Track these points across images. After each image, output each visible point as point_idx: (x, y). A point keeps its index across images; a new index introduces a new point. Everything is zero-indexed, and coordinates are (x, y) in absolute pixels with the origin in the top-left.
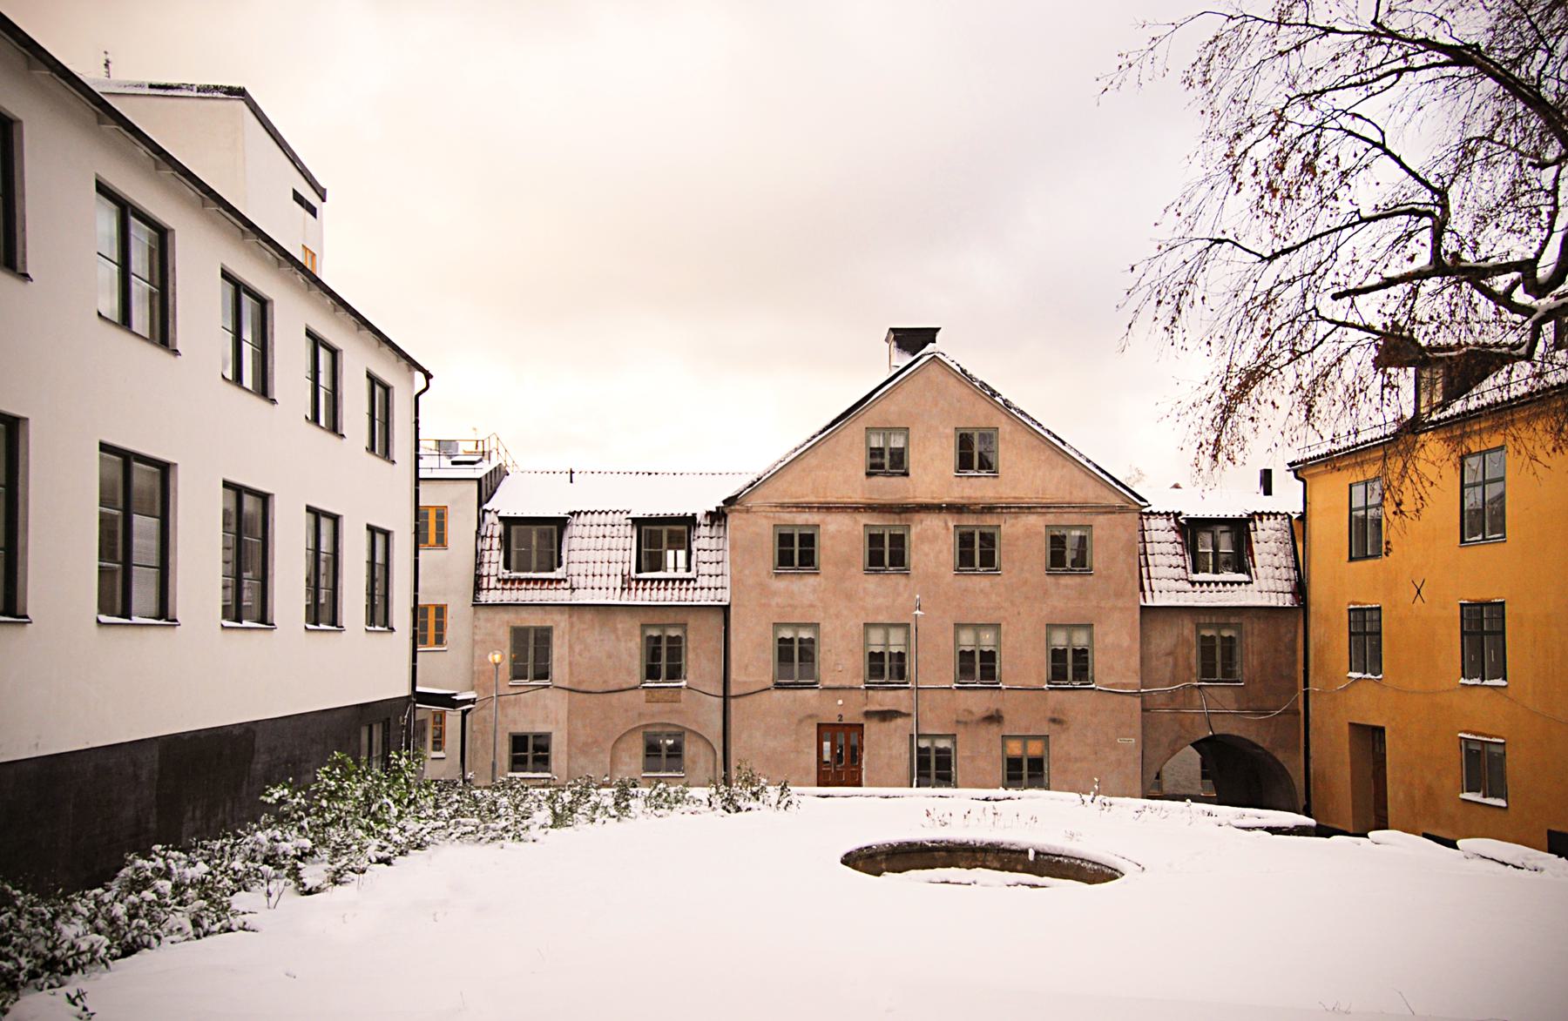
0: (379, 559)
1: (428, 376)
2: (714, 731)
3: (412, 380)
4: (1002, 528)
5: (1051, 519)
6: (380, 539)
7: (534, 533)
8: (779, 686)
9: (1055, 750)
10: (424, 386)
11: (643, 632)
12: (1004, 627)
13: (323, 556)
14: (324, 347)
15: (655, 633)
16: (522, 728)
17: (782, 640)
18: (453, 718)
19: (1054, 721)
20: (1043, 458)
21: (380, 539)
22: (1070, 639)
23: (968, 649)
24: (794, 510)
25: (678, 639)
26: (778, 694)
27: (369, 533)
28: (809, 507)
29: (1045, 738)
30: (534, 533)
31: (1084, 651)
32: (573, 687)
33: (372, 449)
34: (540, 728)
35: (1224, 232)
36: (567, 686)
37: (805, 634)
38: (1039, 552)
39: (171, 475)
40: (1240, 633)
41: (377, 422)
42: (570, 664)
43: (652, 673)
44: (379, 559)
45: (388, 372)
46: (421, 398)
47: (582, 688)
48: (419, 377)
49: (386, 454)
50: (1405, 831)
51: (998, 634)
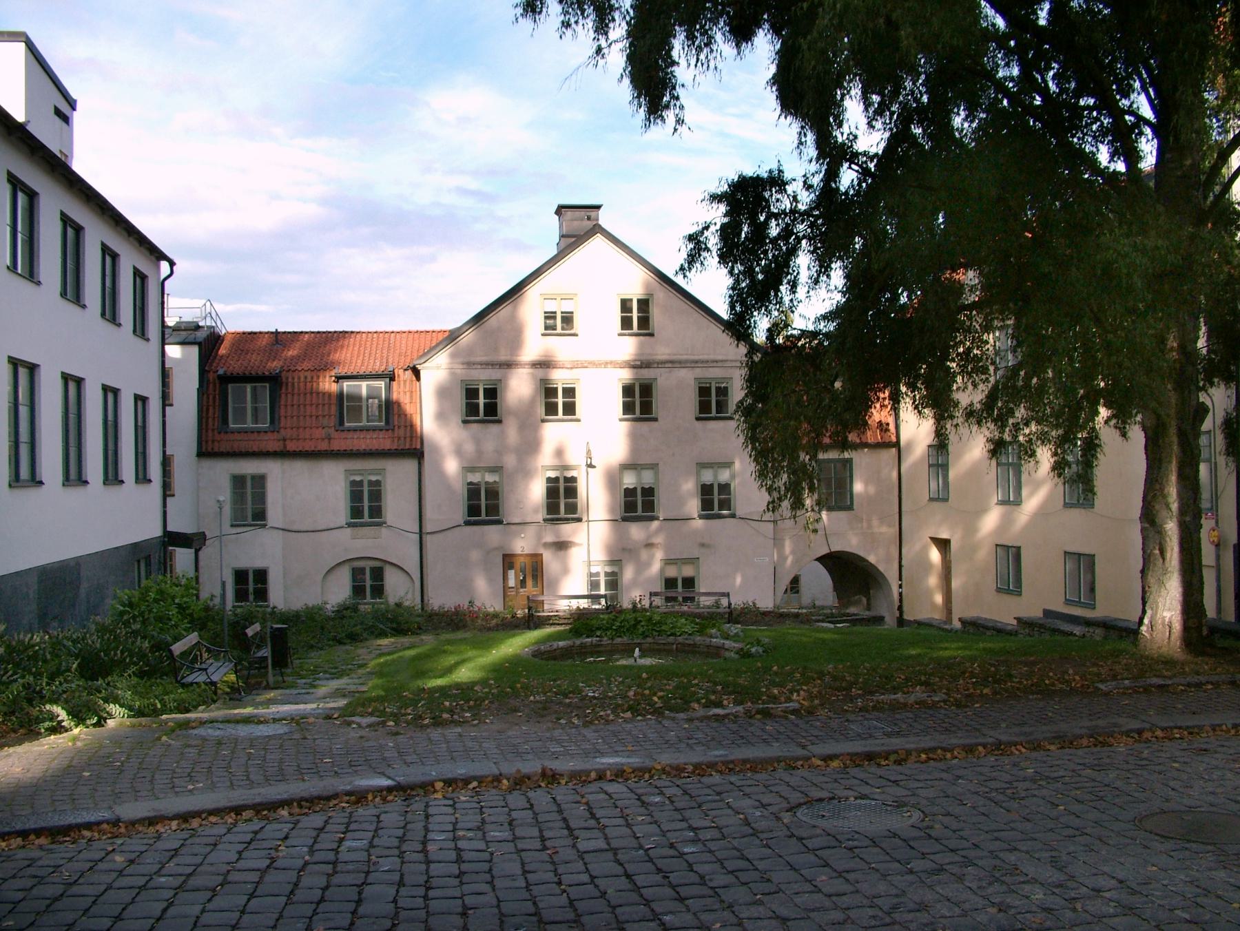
0: (110, 417)
1: (172, 264)
2: (413, 566)
3: (158, 268)
5: (699, 373)
6: (23, 373)
7: (249, 390)
8: (467, 523)
10: (169, 272)
11: (346, 478)
12: (661, 467)
13: (110, 423)
14: (71, 227)
15: (358, 478)
16: (243, 563)
19: (703, 545)
21: (23, 373)
22: (716, 476)
23: (631, 487)
25: (378, 483)
26: (469, 529)
27: (11, 366)
28: (492, 365)
29: (693, 561)
30: (249, 390)
32: (286, 527)
33: (13, 268)
34: (259, 564)
37: (490, 478)
38: (691, 401)
39: (36, 373)
40: (501, 476)
41: (19, 235)
43: (356, 512)
44: (110, 417)
45: (145, 267)
46: (166, 283)
48: (165, 266)
49: (31, 275)
51: (656, 474)
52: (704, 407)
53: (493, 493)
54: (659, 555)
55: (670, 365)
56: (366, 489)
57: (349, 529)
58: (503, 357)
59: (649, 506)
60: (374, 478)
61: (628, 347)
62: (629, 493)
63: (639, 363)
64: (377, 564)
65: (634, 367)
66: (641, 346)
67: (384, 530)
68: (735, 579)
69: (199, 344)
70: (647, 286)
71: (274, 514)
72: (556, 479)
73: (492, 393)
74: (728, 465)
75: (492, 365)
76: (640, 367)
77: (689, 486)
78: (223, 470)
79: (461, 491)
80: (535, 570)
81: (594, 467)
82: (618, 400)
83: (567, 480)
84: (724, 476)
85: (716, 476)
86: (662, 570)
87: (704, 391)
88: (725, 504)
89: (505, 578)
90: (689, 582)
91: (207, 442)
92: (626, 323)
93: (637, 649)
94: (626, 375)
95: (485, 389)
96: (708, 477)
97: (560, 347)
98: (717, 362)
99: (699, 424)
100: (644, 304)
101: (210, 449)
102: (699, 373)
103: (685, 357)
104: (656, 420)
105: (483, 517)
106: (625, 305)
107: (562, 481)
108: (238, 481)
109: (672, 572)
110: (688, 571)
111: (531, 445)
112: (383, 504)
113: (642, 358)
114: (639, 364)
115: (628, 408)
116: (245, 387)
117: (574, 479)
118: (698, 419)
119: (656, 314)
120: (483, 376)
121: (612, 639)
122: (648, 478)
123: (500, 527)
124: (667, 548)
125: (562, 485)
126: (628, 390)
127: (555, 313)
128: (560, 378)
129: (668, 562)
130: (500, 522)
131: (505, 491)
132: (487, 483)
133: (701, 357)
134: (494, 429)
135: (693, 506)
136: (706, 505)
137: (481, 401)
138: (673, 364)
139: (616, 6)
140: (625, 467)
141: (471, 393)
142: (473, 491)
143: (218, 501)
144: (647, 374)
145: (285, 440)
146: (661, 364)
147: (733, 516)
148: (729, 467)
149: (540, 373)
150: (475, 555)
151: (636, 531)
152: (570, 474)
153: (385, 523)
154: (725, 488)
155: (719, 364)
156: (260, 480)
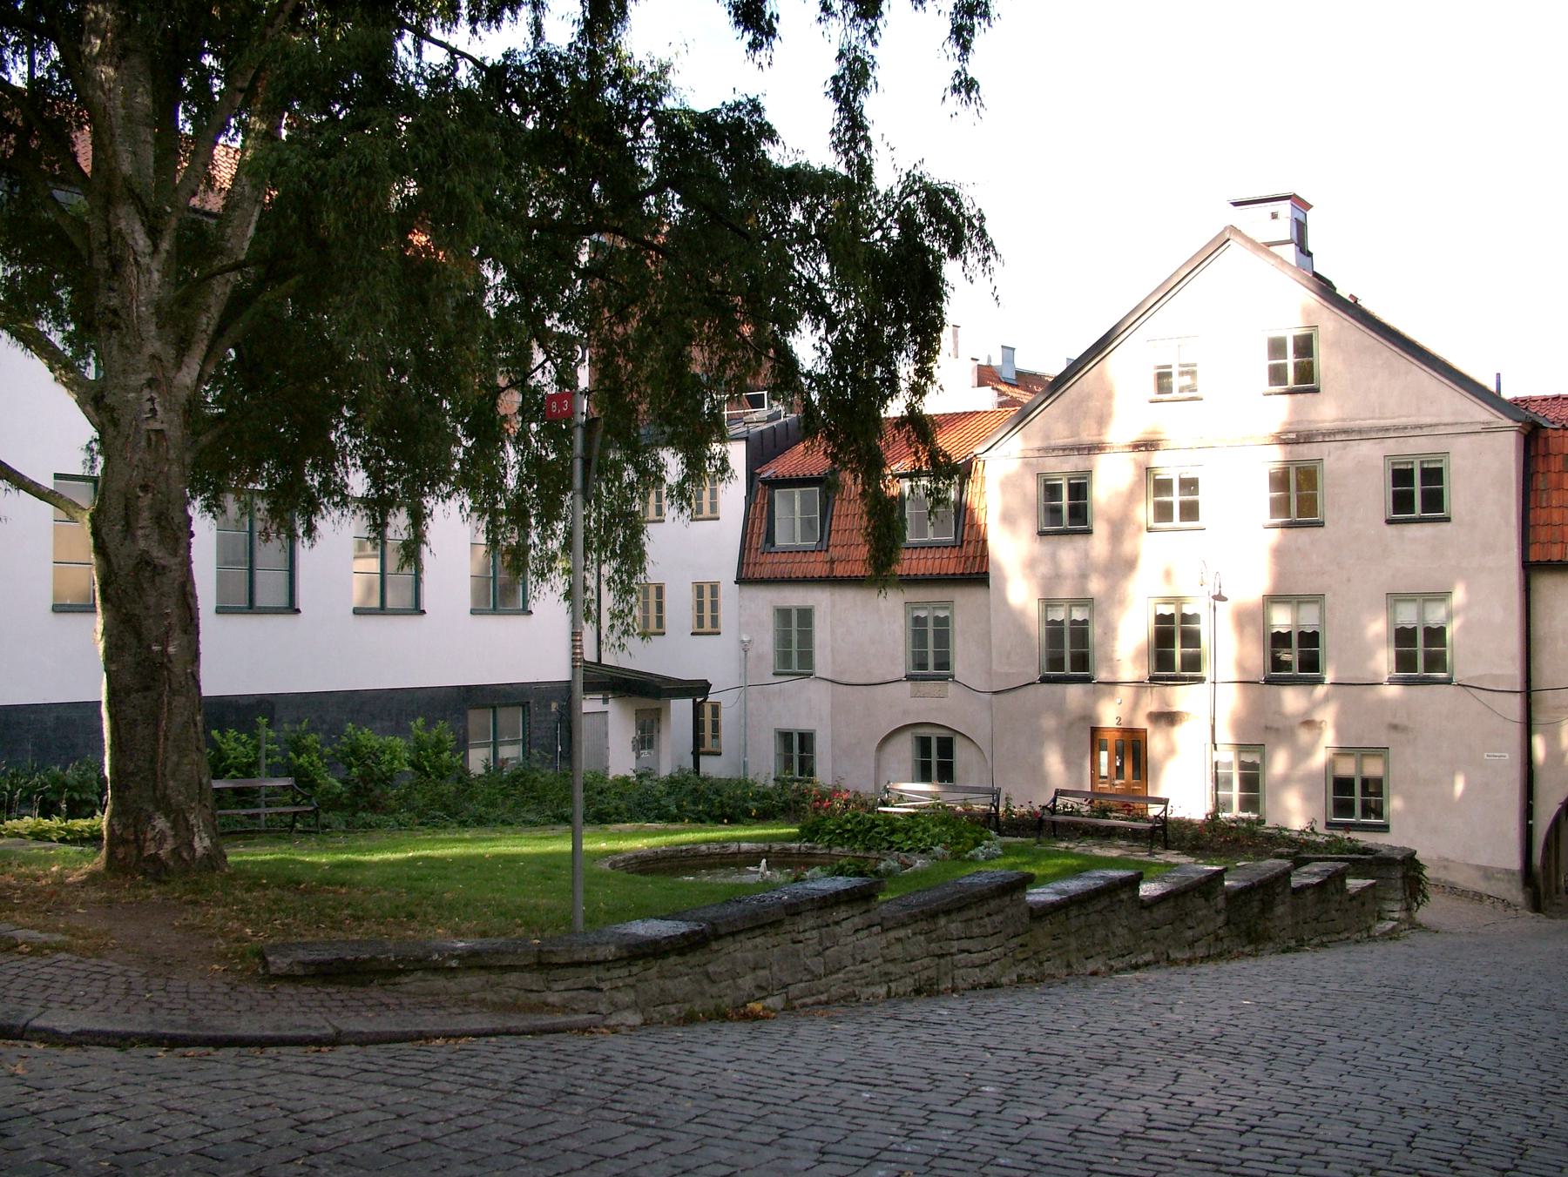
4: (1325, 462)
9: (1396, 771)
11: (906, 613)
15: (923, 614)
17: (1053, 622)
18: (681, 709)
20: (1379, 362)
22: (1421, 613)
23: (1284, 631)
24: (1061, 453)
26: (1046, 687)
28: (1079, 449)
29: (1380, 752)
31: (1315, 635)
34: (804, 726)
35: (1274, 216)
36: (829, 677)
37: (1078, 615)
38: (1379, 492)
42: (832, 651)
47: (845, 680)
50: (198, 634)
52: (1402, 502)
53: (1081, 632)
54: (1328, 738)
55: (1343, 437)
56: (930, 628)
57: (908, 685)
58: (1087, 437)
59: (1311, 663)
60: (942, 614)
61: (1280, 411)
62: (1280, 640)
63: (1293, 436)
64: (944, 733)
65: (1286, 443)
66: (1295, 410)
67: (951, 687)
68: (1452, 783)
69: (747, 439)
70: (1307, 313)
71: (823, 661)
72: (1169, 619)
73: (1080, 490)
74: (1443, 596)
75: (1079, 449)
76: (1296, 442)
77: (1378, 628)
78: (767, 600)
79: (1037, 630)
80: (1133, 747)
81: (1225, 599)
82: (1263, 495)
83: (1185, 618)
84: (1435, 616)
85: (1421, 613)
86: (1330, 765)
87: (1401, 477)
88: (1436, 661)
89: (1095, 763)
90: (1374, 787)
91: (748, 565)
92: (1277, 375)
93: (764, 861)
94: (1276, 456)
95: (1070, 486)
96: (1407, 616)
97: (1166, 420)
98: (1420, 427)
99: (1392, 529)
100: (1305, 346)
101: (750, 575)
102: (1392, 447)
103: (1369, 423)
104: (1321, 524)
105: (1068, 671)
106: (1277, 347)
107: (1177, 619)
108: (783, 614)
109: (1347, 768)
110: (1373, 768)
111: (1121, 566)
112: (951, 650)
113: (1300, 428)
114: (1294, 438)
115: (1279, 507)
116: (793, 493)
117: (1194, 618)
118: (1389, 522)
119: (1325, 360)
120: (1063, 468)
121: (829, 847)
122: (1309, 619)
123: (1089, 686)
124: (1340, 730)
125: (1177, 627)
126: (1280, 481)
127: (1170, 367)
128: (1168, 465)
129: (1343, 752)
130: (1087, 680)
131: (1095, 632)
132: (1074, 622)
133: (1396, 422)
134: (1079, 541)
135: (1384, 661)
136: (1405, 662)
137: (1065, 502)
138: (1344, 434)
139: (123, 64)
140: (1273, 599)
141: (1052, 491)
142: (1054, 632)
143: (742, 642)
144: (1307, 452)
145: (832, 562)
146: (1329, 435)
147: (1448, 682)
148: (1443, 600)
149: (1141, 456)
150: (1049, 723)
151: (1292, 699)
152: (1188, 610)
153: (953, 677)
154: (1436, 635)
155: (1426, 431)
156: (806, 615)
